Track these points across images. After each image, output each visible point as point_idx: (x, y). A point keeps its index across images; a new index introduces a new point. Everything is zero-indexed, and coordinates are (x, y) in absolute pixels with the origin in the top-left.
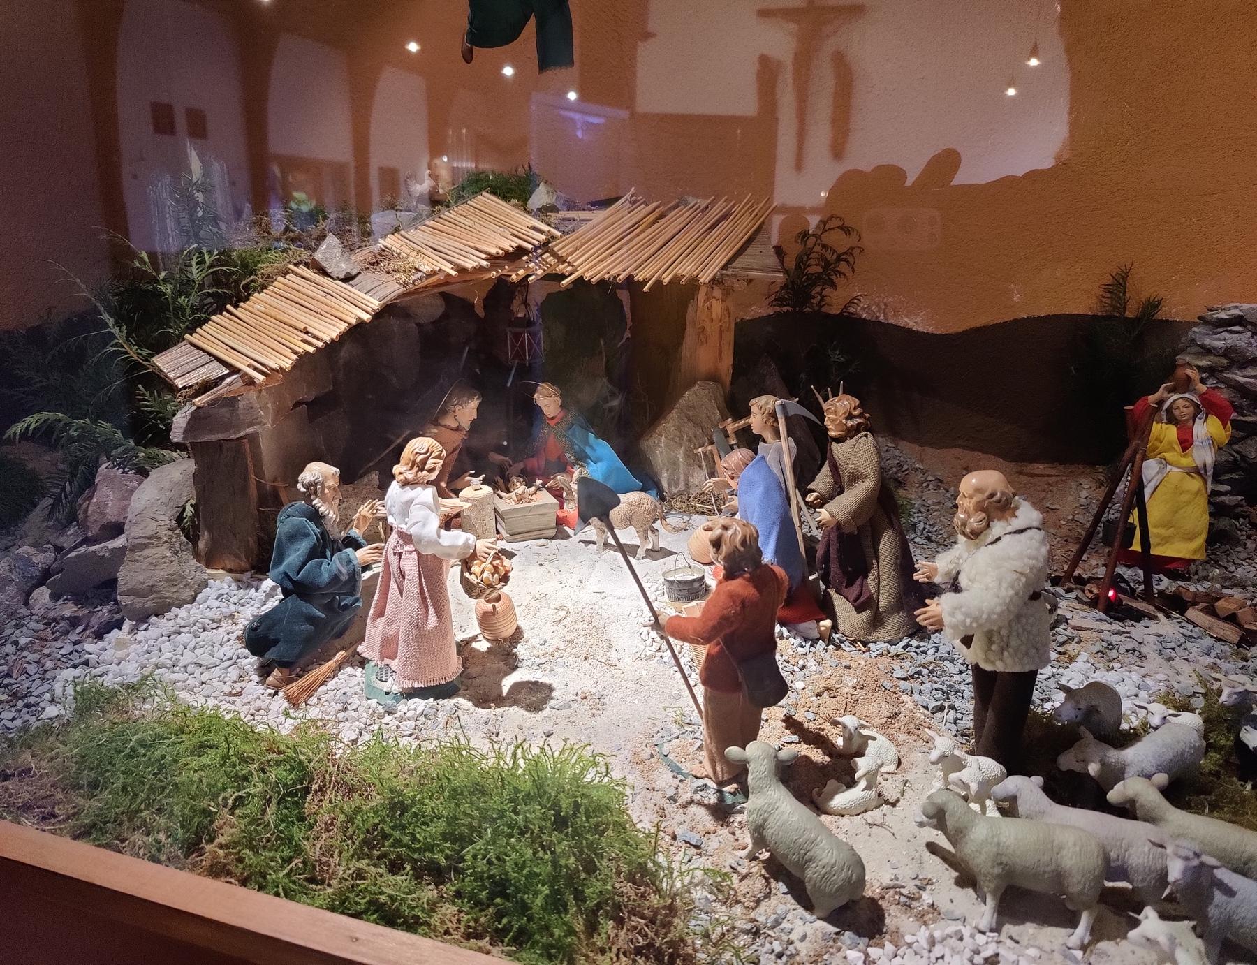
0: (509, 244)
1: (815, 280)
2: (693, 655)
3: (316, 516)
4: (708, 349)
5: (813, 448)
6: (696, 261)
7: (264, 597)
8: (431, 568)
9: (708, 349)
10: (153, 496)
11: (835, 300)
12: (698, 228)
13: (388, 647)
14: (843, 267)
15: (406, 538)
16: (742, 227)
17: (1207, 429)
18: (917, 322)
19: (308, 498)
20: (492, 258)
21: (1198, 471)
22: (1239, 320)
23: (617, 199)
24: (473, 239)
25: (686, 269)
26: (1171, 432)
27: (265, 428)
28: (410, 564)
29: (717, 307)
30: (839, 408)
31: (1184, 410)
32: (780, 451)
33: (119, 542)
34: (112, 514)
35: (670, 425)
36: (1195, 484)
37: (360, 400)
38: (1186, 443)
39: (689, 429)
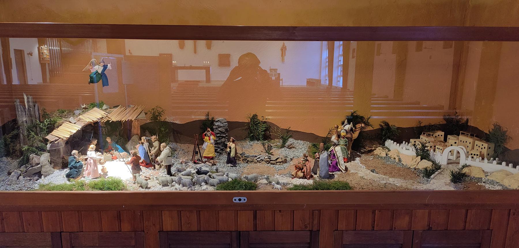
0: (101, 116)
1: (157, 116)
2: (130, 167)
3: (75, 158)
4: (136, 130)
5: (151, 145)
6: (132, 117)
7: (67, 171)
8: (95, 161)
9: (136, 130)
10: (45, 158)
11: (162, 119)
12: (132, 111)
13: (89, 174)
14: (162, 113)
15: (91, 158)
16: (140, 110)
17: (212, 137)
18: (177, 122)
19: (73, 155)
20: (98, 119)
21: (212, 144)
22: (219, 121)
23: (118, 106)
24: (94, 115)
25: (130, 118)
26: (208, 138)
27: (62, 147)
28: (92, 161)
29: (136, 123)
30: (153, 138)
31: (209, 135)
32: (146, 145)
33: (39, 166)
34: (37, 162)
35: (130, 142)
36: (212, 145)
37: (78, 142)
38: (210, 139)
39: (133, 143)
